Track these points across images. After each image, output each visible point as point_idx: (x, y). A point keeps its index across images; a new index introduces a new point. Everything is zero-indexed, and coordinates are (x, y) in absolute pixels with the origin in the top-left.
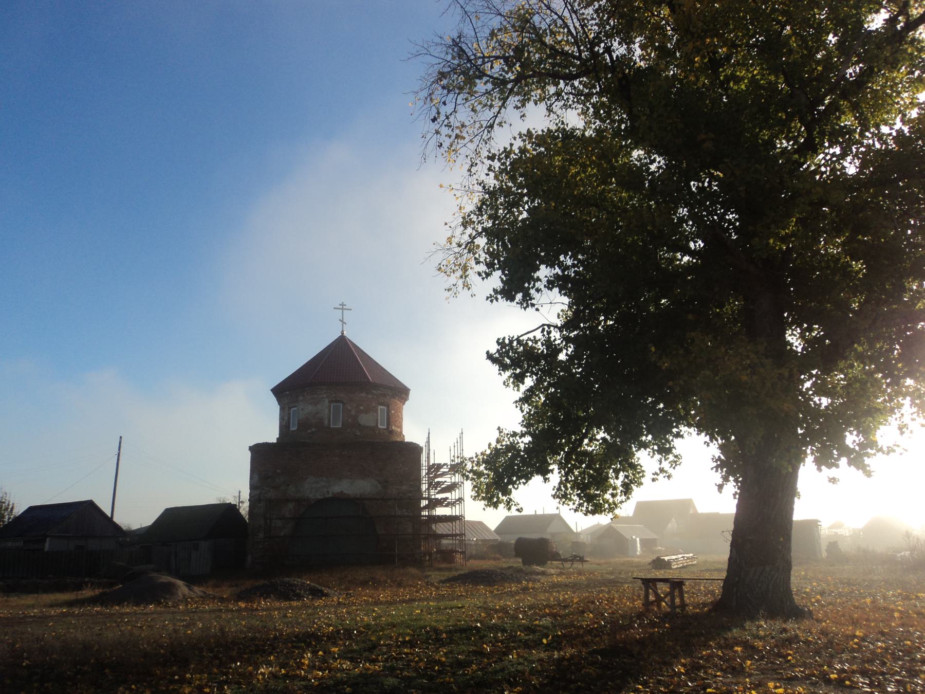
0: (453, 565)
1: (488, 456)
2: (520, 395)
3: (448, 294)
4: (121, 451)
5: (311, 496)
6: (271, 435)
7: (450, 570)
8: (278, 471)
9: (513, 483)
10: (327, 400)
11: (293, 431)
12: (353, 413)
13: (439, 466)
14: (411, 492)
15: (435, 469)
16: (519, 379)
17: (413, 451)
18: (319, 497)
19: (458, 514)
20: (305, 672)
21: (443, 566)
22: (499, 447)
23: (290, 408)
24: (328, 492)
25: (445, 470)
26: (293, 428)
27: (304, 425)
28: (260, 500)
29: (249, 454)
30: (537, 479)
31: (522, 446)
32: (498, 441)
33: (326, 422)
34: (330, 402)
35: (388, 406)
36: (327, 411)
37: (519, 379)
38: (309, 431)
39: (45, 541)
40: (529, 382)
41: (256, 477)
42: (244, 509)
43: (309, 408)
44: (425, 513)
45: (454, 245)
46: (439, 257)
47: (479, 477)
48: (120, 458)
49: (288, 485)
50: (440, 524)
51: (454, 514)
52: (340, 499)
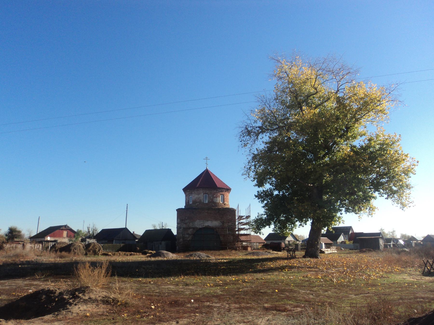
0: (247, 251)
1: (255, 220)
2: (263, 205)
3: (244, 180)
4: (128, 209)
5: (198, 227)
6: (182, 205)
7: (246, 252)
8: (186, 218)
9: (262, 228)
10: (202, 193)
11: (190, 204)
12: (212, 198)
13: (242, 217)
14: (232, 225)
15: (241, 217)
16: (262, 201)
17: (232, 212)
18: (201, 227)
19: (249, 233)
20: (320, 163)
21: (243, 251)
22: (258, 218)
23: (189, 196)
24: (204, 225)
25: (244, 217)
26: (191, 203)
27: (194, 202)
28: (180, 228)
29: (176, 212)
30: (268, 227)
31: (264, 218)
32: (258, 216)
33: (202, 201)
34: (204, 194)
35: (224, 195)
36: (202, 197)
37: (262, 201)
38: (197, 204)
39: (113, 241)
40: (265, 202)
41: (179, 220)
42: (175, 232)
43: (196, 196)
44: (237, 233)
45: (246, 168)
46: (243, 171)
47: (253, 226)
48: (127, 212)
49: (190, 223)
50: (243, 237)
51: (247, 233)
52: (207, 228)
